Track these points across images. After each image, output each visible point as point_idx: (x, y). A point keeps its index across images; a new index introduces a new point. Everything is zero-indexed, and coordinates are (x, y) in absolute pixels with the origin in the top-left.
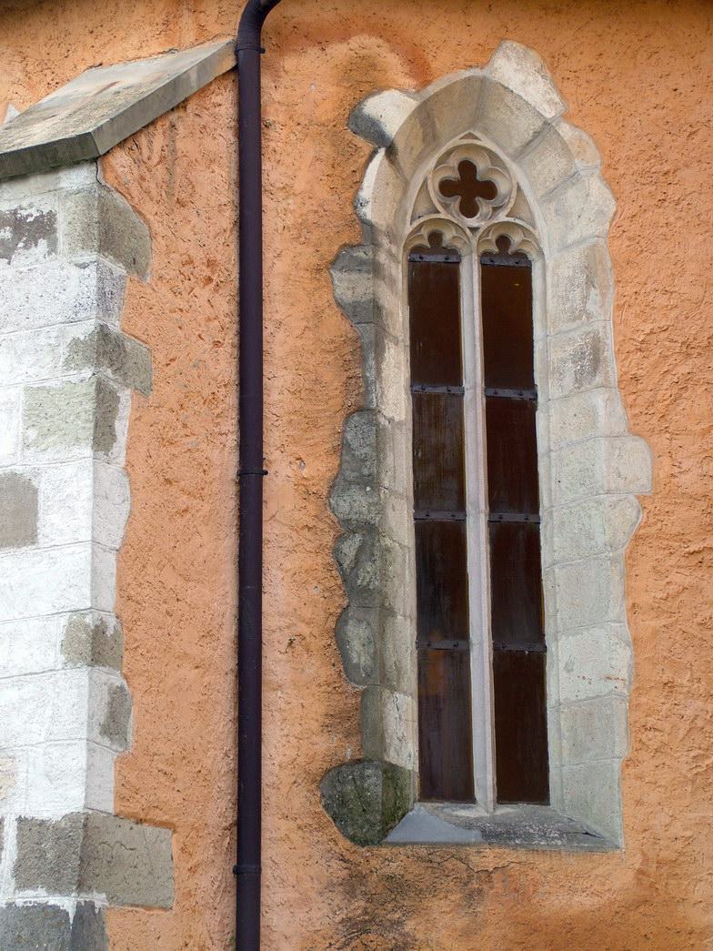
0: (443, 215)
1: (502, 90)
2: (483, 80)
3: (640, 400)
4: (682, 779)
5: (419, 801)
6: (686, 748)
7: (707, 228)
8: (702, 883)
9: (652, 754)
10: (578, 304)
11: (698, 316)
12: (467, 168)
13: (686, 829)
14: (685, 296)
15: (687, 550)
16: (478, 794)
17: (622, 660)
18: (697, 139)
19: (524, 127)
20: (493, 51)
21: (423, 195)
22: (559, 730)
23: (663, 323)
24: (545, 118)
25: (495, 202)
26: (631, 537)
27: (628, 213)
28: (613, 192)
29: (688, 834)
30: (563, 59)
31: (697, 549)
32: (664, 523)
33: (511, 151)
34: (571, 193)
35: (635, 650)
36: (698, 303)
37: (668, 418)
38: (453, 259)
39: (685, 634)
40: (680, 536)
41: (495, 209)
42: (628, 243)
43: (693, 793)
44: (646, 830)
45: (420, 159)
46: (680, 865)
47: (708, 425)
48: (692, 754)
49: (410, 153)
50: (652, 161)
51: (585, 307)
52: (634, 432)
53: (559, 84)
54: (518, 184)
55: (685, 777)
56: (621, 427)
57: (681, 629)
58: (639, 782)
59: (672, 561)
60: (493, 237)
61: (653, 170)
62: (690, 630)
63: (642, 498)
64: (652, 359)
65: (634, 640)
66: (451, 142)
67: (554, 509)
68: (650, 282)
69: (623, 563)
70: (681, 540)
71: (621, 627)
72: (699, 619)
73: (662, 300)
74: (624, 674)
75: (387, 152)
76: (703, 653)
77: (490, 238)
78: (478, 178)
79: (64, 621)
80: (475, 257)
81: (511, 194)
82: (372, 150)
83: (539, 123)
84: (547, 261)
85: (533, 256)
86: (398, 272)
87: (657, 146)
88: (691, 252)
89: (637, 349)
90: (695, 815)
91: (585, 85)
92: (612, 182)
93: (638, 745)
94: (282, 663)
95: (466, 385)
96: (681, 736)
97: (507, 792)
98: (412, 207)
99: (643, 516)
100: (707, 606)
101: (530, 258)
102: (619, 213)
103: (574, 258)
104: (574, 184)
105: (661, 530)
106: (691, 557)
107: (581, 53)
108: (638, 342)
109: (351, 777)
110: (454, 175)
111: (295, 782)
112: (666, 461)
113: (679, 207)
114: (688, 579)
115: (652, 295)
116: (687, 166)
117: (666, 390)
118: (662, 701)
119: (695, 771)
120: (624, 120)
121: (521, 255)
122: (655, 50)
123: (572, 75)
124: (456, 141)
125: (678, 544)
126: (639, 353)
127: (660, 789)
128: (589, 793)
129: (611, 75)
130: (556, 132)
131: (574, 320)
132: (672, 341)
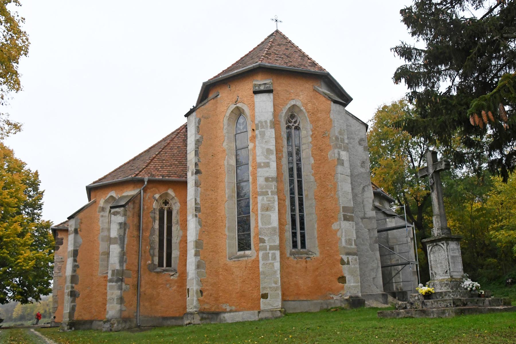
12: (166, 201)
17: (178, 253)
19: (171, 197)
52: (181, 230)
53: (175, 193)
79: (473, 16)
86: (158, 213)
92: (180, 203)
97: (167, 266)
103: (176, 211)
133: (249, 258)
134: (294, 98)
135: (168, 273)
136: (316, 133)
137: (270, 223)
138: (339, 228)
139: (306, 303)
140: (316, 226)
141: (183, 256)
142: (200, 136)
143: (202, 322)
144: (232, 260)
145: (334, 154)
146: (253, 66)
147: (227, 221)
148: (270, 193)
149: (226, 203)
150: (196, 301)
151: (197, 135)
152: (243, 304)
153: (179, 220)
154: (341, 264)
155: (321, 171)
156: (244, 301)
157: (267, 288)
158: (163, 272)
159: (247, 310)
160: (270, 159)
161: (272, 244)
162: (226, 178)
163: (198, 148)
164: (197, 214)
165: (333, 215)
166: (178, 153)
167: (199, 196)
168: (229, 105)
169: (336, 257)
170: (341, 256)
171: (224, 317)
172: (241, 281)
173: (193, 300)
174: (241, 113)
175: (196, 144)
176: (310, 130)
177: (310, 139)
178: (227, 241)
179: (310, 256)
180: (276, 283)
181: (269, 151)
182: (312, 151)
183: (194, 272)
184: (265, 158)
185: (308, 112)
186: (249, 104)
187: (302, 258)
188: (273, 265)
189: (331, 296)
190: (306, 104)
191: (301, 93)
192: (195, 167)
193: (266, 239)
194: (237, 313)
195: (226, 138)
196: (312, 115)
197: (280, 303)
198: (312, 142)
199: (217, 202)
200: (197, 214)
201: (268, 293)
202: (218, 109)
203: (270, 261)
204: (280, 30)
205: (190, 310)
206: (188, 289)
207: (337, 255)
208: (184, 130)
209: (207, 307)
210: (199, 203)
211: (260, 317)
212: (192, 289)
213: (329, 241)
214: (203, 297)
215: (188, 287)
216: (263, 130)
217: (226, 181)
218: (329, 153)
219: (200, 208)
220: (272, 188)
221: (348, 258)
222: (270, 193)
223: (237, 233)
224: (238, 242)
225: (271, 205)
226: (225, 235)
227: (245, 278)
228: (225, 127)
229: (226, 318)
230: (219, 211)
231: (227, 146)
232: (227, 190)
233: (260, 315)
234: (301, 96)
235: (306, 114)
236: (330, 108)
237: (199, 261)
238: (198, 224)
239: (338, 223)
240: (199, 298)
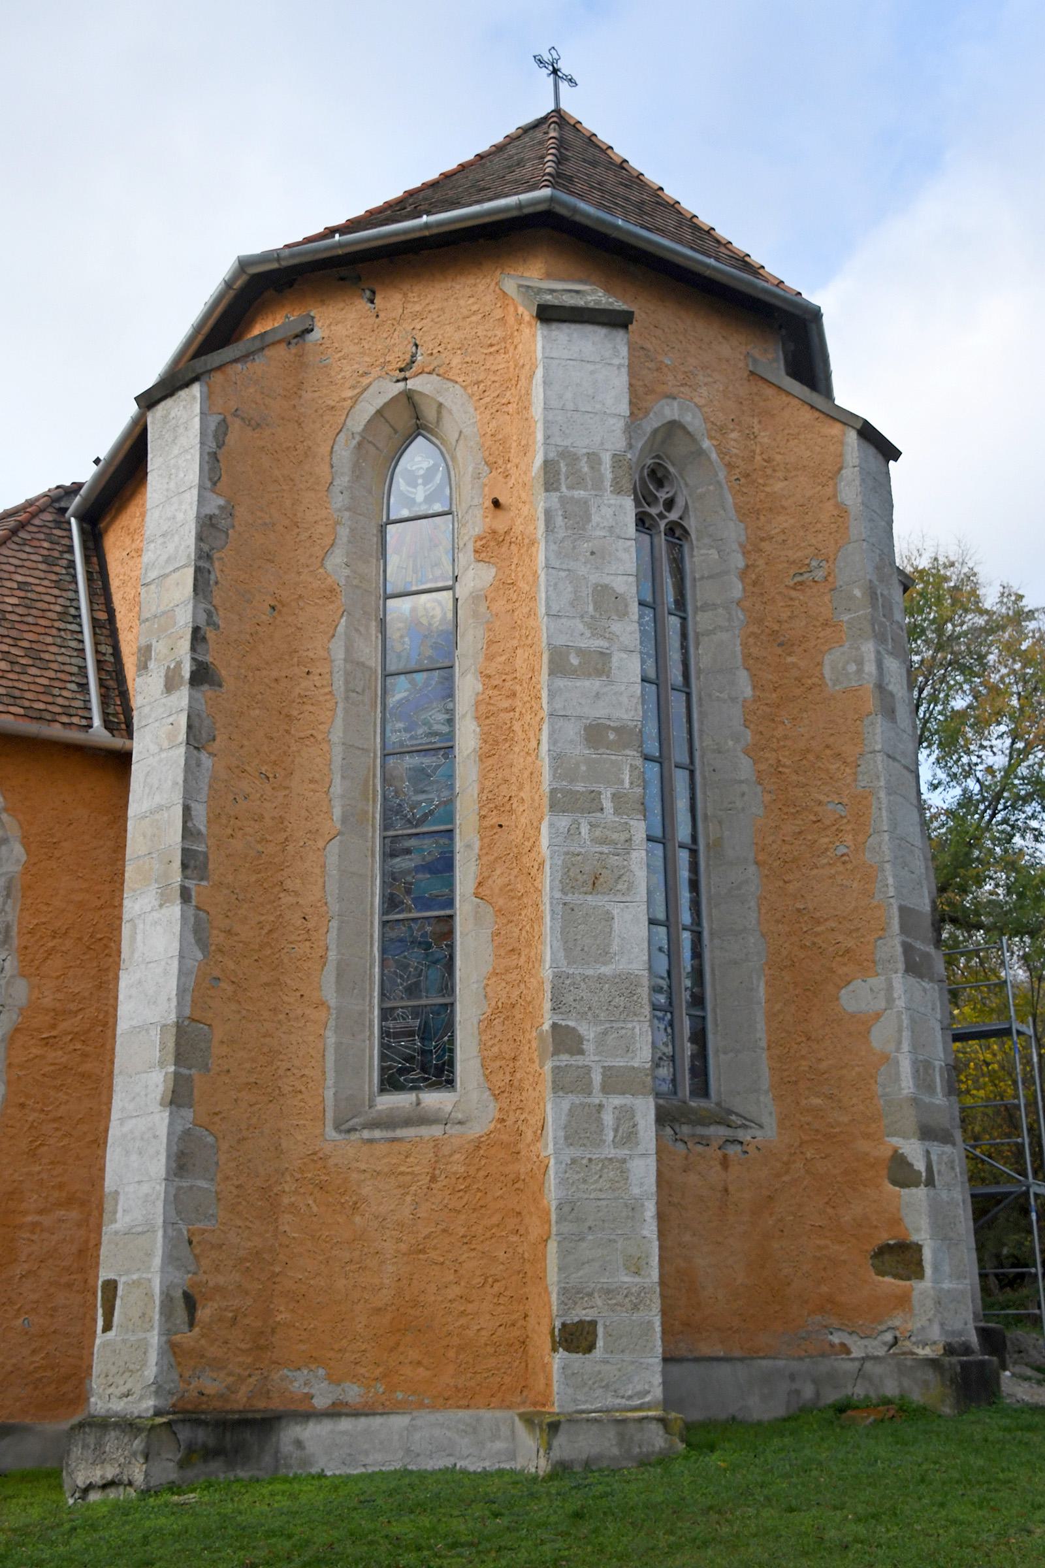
36: (64, 910)
40: (38, 1030)
52: (23, 975)
59: (33, 1041)
63: (21, 1009)
73: (45, 908)
92: (26, 846)
133: (453, 1130)
134: (675, 391)
136: (761, 562)
137: (605, 955)
138: (883, 1005)
139: (725, 1369)
140: (762, 992)
141: (22, 1106)
142: (221, 502)
143: (190, 1473)
144: (354, 1136)
145: (860, 663)
146: (520, 206)
147: (333, 934)
148: (608, 805)
149: (334, 847)
150: (161, 1354)
151: (208, 494)
152: (407, 1370)
154: (895, 1183)
155: (786, 737)
156: (414, 1355)
157: (590, 1295)
159: (433, 1408)
160: (611, 638)
161: (619, 1062)
162: (339, 722)
163: (209, 557)
164: (190, 884)
165: (851, 943)
166: (20, 610)
167: (203, 797)
168: (365, 381)
169: (863, 1146)
170: (895, 1141)
171: (299, 1444)
172: (403, 1247)
173: (143, 1346)
174: (418, 427)
175: (200, 538)
176: (735, 546)
177: (737, 590)
178: (331, 1039)
179: (741, 1134)
180: (636, 1267)
181: (604, 596)
182: (745, 645)
183: (161, 1188)
184: (588, 633)
185: (730, 466)
186: (478, 383)
187: (705, 1142)
188: (624, 1173)
189: (836, 1339)
190: (722, 430)
191: (701, 378)
192: (193, 649)
193: (588, 1031)
194: (377, 1421)
195: (344, 532)
196: (743, 480)
197: (657, 1379)
198: (747, 604)
199: (281, 837)
200: (190, 884)
201: (593, 1324)
202: (308, 396)
203: (611, 1152)
204: (566, 106)
205: (118, 1406)
206: (111, 1287)
207: (867, 1136)
208: (47, 516)
209: (212, 1384)
210: (203, 829)
211: (556, 1454)
212: (137, 1283)
213: (823, 1066)
214: (197, 1329)
215: (105, 1274)
216: (580, 494)
217: (337, 735)
218: (828, 659)
219: (206, 855)
220: (622, 782)
221: (928, 1152)
222: (608, 805)
223: (376, 1001)
224: (382, 1045)
225: (614, 860)
226: (321, 1004)
227: (426, 1232)
228: (343, 481)
229: (311, 1447)
230: (288, 884)
231: (347, 572)
232: (337, 780)
233: (555, 1443)
234: (704, 391)
235: (722, 475)
236: (841, 455)
237: (187, 1132)
238: (191, 938)
239: (877, 982)
240: (177, 1338)
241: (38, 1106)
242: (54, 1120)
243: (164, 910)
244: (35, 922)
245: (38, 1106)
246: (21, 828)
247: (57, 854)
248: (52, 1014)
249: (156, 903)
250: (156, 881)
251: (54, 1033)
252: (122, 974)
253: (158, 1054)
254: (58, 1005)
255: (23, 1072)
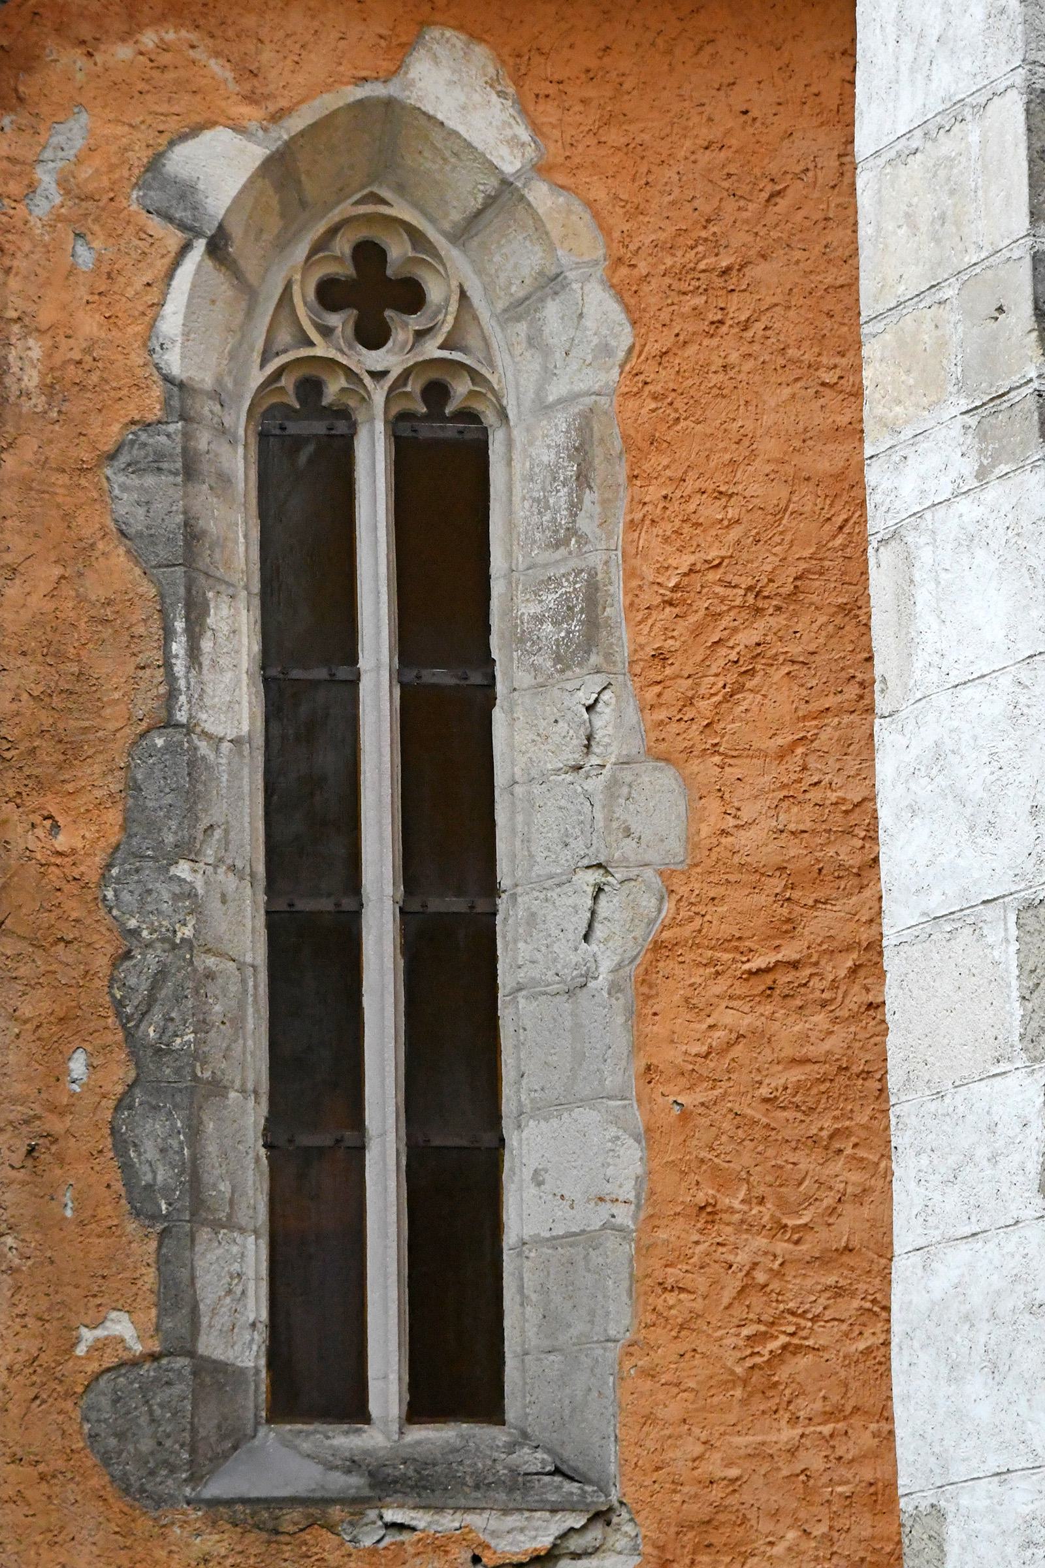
0: (321, 350)
1: (423, 121)
2: (389, 103)
3: (668, 695)
4: (725, 1377)
5: (269, 1421)
6: (736, 1321)
7: (798, 373)
8: (756, 1559)
9: (674, 1333)
10: (563, 518)
11: (777, 539)
13: (729, 1465)
14: (756, 501)
15: (747, 966)
16: (374, 1407)
18: (783, 204)
20: (407, 48)
21: (285, 312)
22: (521, 1289)
23: (713, 554)
24: (502, 172)
25: (416, 322)
26: (648, 945)
27: (653, 348)
28: (627, 309)
29: (733, 1472)
30: (537, 59)
31: (763, 966)
32: (708, 918)
33: (447, 226)
34: (552, 310)
35: (649, 1148)
36: (780, 512)
37: (718, 727)
38: (341, 427)
39: (738, 1118)
40: (731, 943)
41: (420, 335)
42: (653, 405)
43: (744, 1402)
44: (658, 1469)
45: (282, 244)
46: (716, 1528)
47: (790, 738)
48: (745, 1332)
49: (257, 239)
50: (700, 248)
51: (574, 521)
54: (461, 286)
55: (732, 1373)
56: (634, 746)
57: (731, 1110)
58: (649, 1384)
59: (720, 986)
60: (413, 387)
61: (702, 266)
62: (749, 1111)
63: (666, 875)
64: (692, 619)
65: (648, 1130)
66: (336, 211)
67: (519, 890)
68: (692, 475)
69: (630, 992)
70: (736, 948)
71: (625, 1107)
72: (764, 1091)
73: (712, 511)
74: (628, 1191)
75: (208, 244)
76: (770, 1152)
77: (409, 389)
78: (389, 272)
80: (380, 426)
81: (447, 306)
82: (184, 242)
83: (494, 182)
84: (515, 433)
85: (490, 418)
87: (708, 221)
88: (768, 419)
89: (664, 602)
90: (750, 1439)
91: (579, 107)
93: (650, 1318)
94: (15, 1186)
95: (363, 664)
96: (726, 1301)
98: (263, 337)
99: (668, 906)
100: (780, 1067)
101: (486, 422)
102: (637, 348)
104: (556, 293)
105: (700, 931)
106: (754, 980)
107: (571, 46)
108: (667, 588)
109: (137, 1385)
110: (345, 270)
111: (36, 1398)
112: (713, 805)
113: (749, 334)
114: (748, 1020)
115: (696, 499)
116: (764, 257)
117: (717, 675)
118: (695, 1237)
119: (749, 1363)
120: (649, 172)
121: (469, 416)
122: (711, 36)
123: (552, 90)
124: (345, 209)
125: (731, 956)
126: (668, 609)
127: (685, 1395)
128: (567, 1402)
129: (627, 86)
130: (522, 198)
131: (557, 546)
132: (729, 585)
135: (449, 1522)
141: (708, 1212)
153: (617, 591)
158: (357, 1504)
241: (767, 1212)
242: (823, 1260)
243: (994, 493)
244: (685, 561)
245: (767, 1212)
246: (605, 229)
247: (739, 308)
248: (776, 884)
249: (968, 467)
250: (961, 386)
251: (790, 952)
252: (883, 731)
253: (1017, 1010)
254: (795, 849)
255: (701, 1095)
